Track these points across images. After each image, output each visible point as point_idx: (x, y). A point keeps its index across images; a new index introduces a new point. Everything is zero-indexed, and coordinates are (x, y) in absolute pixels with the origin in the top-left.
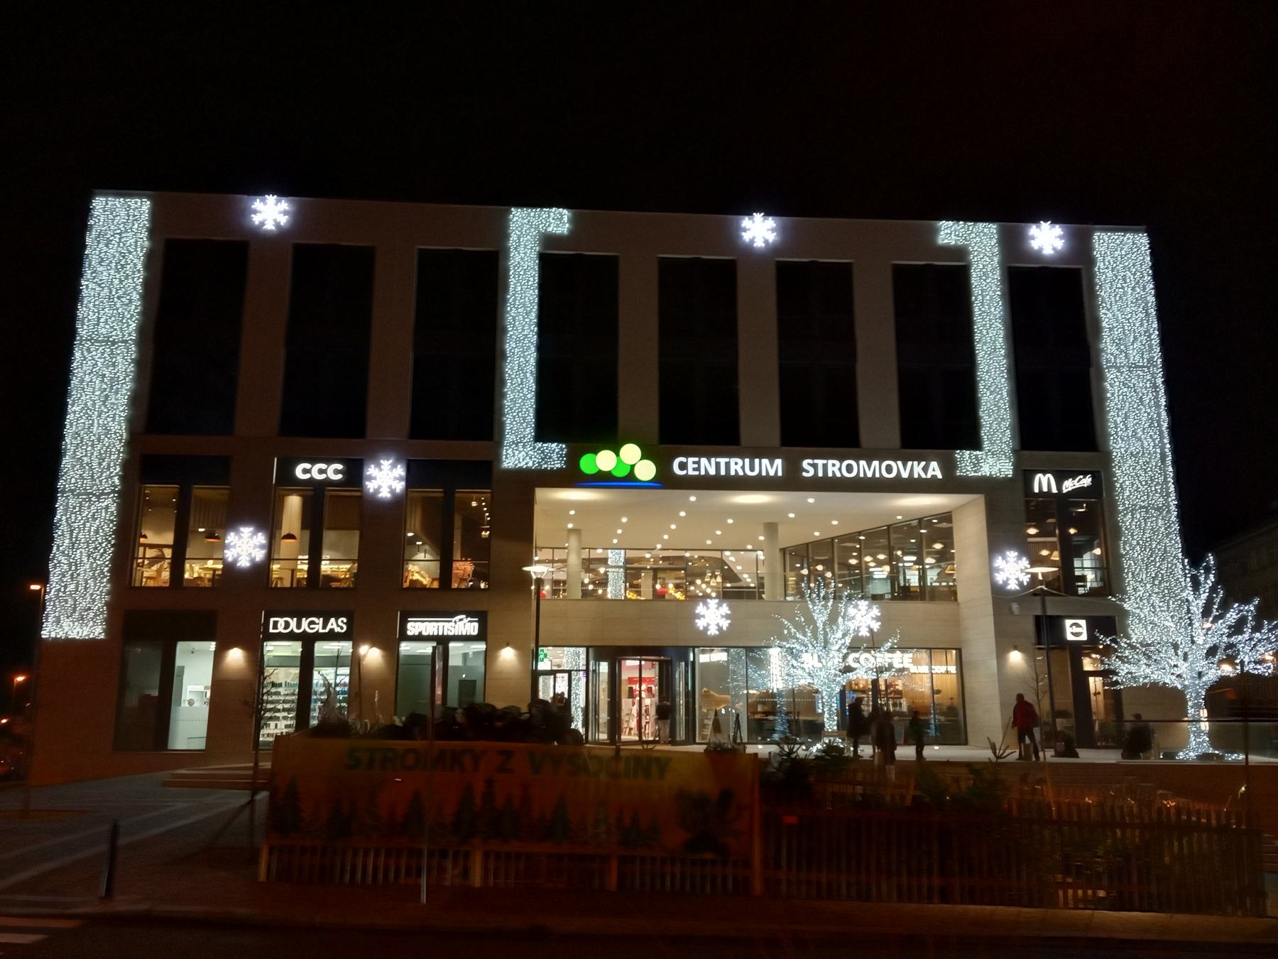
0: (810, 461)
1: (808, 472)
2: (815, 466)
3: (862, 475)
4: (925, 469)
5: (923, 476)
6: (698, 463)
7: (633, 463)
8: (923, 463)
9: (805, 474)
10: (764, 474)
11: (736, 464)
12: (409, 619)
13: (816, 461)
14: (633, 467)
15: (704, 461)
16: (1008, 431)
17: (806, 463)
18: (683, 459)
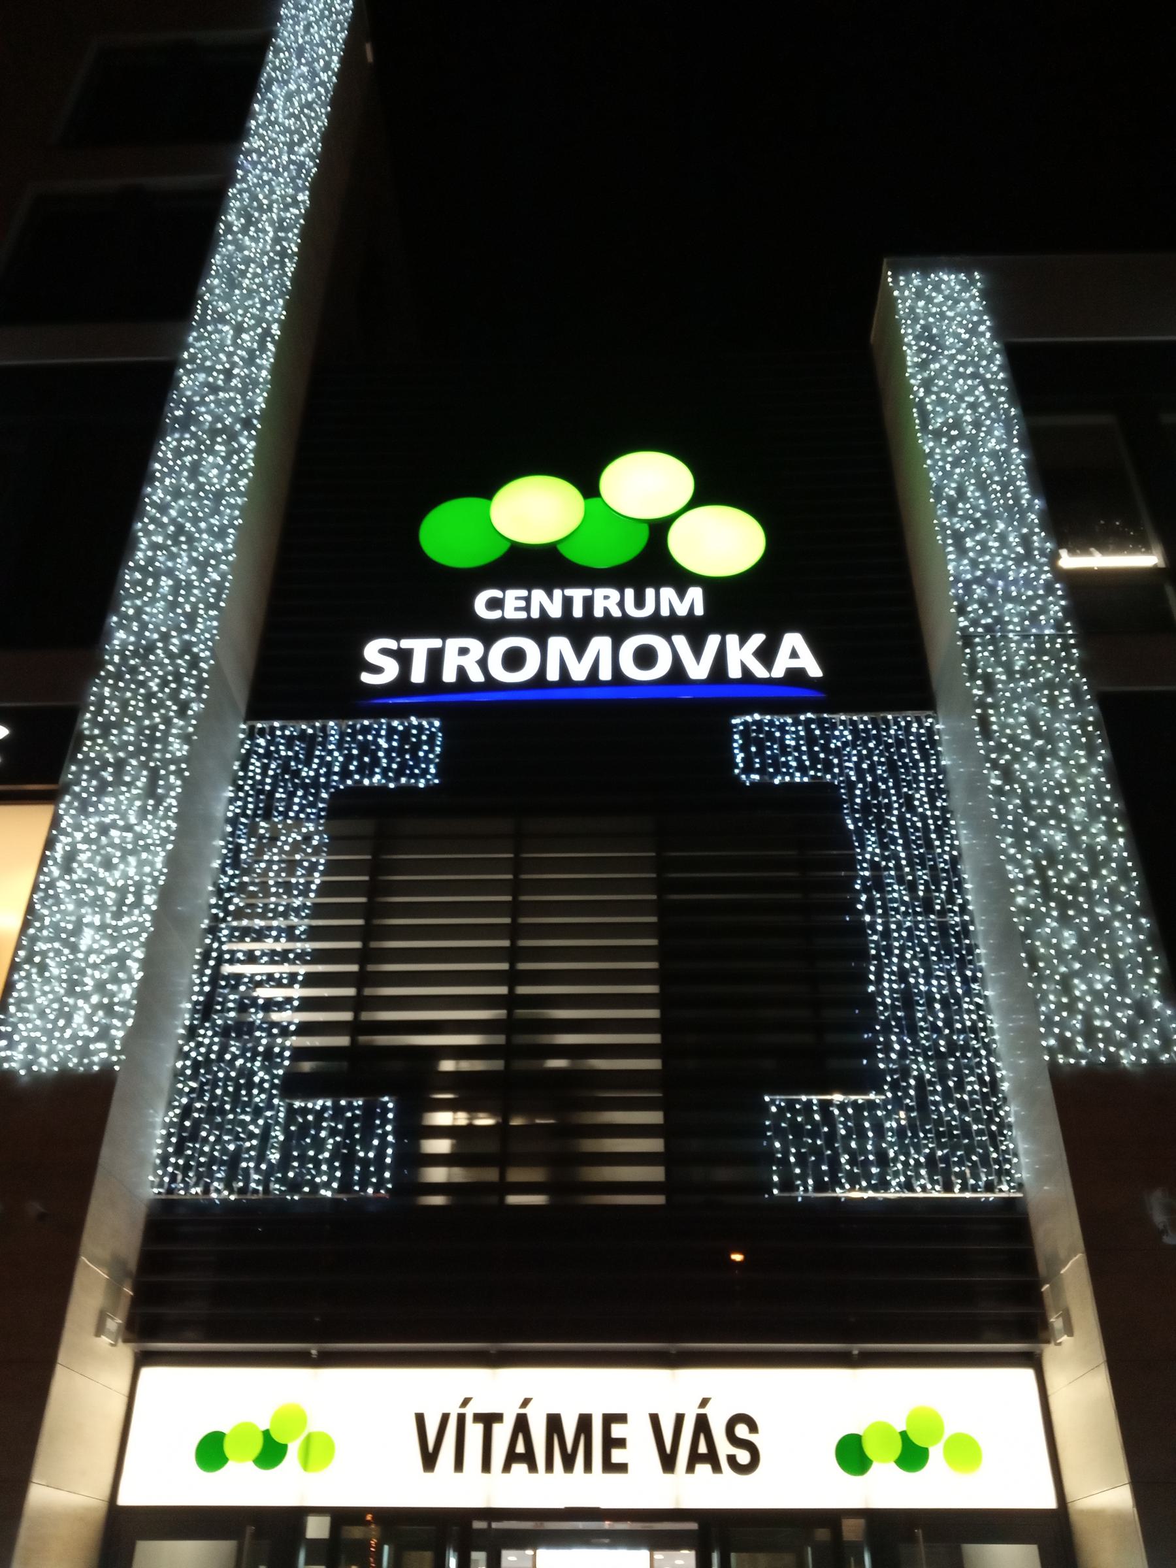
0: (391, 644)
1: (377, 670)
2: (404, 658)
3: (553, 675)
4: (766, 655)
5: (760, 671)
6: (528, 599)
7: (658, 512)
8: (758, 639)
9: (366, 678)
10: (553, 675)
11: (463, 651)
12: (659, 1200)
13: (406, 643)
14: (659, 529)
15: (538, 595)
16: (939, 512)
17: (372, 651)
18: (496, 593)
